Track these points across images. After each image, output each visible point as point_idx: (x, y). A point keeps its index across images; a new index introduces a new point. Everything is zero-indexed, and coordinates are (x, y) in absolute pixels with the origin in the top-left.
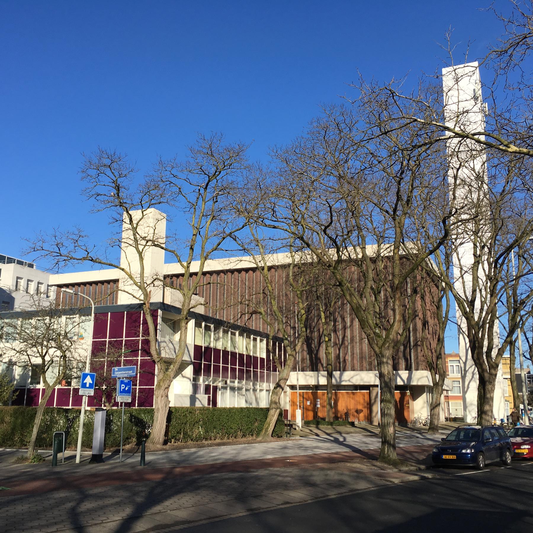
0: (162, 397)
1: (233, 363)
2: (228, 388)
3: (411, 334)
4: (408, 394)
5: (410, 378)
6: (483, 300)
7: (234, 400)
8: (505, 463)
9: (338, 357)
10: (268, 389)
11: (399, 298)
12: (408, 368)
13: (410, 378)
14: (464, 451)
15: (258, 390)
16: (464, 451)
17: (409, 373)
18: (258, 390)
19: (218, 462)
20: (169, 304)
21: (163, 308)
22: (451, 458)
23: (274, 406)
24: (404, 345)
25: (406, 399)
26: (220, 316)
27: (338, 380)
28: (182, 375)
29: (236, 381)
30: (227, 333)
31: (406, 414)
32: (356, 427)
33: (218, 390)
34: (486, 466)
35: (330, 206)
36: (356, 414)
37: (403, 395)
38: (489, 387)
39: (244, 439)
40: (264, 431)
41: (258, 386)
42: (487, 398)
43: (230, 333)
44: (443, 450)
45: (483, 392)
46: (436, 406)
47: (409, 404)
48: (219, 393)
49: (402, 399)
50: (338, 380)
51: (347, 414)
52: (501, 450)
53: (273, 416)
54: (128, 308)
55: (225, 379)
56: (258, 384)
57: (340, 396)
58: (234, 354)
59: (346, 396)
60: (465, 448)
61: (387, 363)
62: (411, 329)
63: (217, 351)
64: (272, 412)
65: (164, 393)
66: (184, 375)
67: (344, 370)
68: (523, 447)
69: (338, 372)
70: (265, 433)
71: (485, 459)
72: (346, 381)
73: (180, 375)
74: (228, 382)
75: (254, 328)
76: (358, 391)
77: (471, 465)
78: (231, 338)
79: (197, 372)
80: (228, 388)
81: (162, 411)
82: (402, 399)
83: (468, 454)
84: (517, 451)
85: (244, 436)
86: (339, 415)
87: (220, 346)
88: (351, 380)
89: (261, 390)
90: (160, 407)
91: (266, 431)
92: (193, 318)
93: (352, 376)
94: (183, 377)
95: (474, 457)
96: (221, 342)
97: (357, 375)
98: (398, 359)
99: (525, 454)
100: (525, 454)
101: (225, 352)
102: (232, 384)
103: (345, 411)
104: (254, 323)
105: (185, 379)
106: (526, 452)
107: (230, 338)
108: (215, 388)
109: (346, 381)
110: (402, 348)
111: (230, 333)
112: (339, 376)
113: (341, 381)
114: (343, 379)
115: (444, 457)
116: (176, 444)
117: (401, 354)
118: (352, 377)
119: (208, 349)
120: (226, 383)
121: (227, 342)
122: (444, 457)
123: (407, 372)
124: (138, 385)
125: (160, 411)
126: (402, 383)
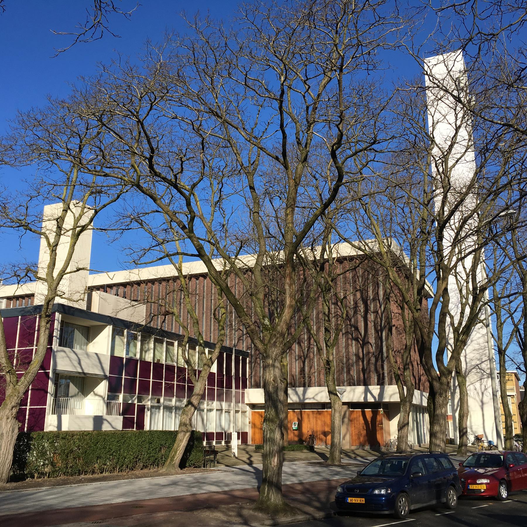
0: (8, 418)
1: (169, 378)
2: (162, 408)
3: (384, 343)
4: (381, 413)
5: (381, 394)
6: (464, 300)
7: (171, 422)
8: (447, 506)
9: (302, 371)
10: (219, 408)
11: (290, 274)
12: (381, 383)
13: (381, 394)
14: (377, 492)
15: (205, 410)
16: (377, 492)
17: (380, 388)
18: (205, 410)
19: (37, 507)
20: (97, 312)
21: (62, 310)
22: (359, 502)
23: (184, 429)
24: (375, 357)
25: (379, 418)
26: (168, 328)
27: (302, 398)
28: (94, 392)
29: (174, 400)
30: (162, 343)
31: (379, 437)
32: (315, 452)
33: (146, 410)
34: (412, 512)
35: (139, 121)
36: (322, 436)
37: (375, 414)
38: (439, 400)
39: (145, 471)
40: (169, 460)
41: (205, 405)
42: (437, 415)
43: (165, 343)
44: (350, 489)
45: (432, 407)
46: (404, 426)
47: (382, 424)
48: (148, 414)
49: (374, 418)
50: (302, 398)
51: (312, 437)
52: (439, 490)
53: (181, 441)
54: (23, 312)
55: (158, 397)
56: (206, 402)
57: (305, 417)
58: (170, 368)
59: (311, 415)
60: (379, 487)
61: (273, 366)
62: (384, 338)
63: (145, 365)
64: (180, 436)
65: (10, 414)
66: (96, 392)
67: (310, 386)
68: (479, 482)
69: (302, 389)
70: (170, 463)
71: (411, 502)
72: (310, 399)
73: (92, 393)
74: (162, 400)
75: (212, 342)
76: (326, 410)
77: (387, 512)
78: (167, 351)
79: (113, 390)
80: (162, 408)
81: (8, 437)
82: (374, 418)
83: (382, 495)
84: (471, 487)
85: (145, 467)
86: (304, 439)
87: (149, 357)
88: (316, 398)
89: (210, 410)
90: (4, 432)
91: (172, 460)
92: (109, 324)
93: (316, 393)
94: (96, 395)
95: (391, 502)
96: (152, 353)
97: (322, 392)
98: (370, 372)
99: (482, 490)
100: (482, 490)
101: (158, 366)
102: (167, 403)
103: (310, 433)
104: (212, 335)
105: (97, 397)
106: (483, 488)
107: (165, 349)
108: (142, 409)
109: (310, 399)
110: (373, 360)
111: (165, 343)
112: (302, 392)
113: (304, 399)
114: (306, 397)
115: (349, 500)
116: (40, 480)
117: (372, 368)
118: (317, 395)
119: (131, 361)
120: (158, 401)
121: (162, 353)
122: (349, 500)
123: (379, 387)
124: (28, 404)
125: (5, 438)
126: (372, 400)
